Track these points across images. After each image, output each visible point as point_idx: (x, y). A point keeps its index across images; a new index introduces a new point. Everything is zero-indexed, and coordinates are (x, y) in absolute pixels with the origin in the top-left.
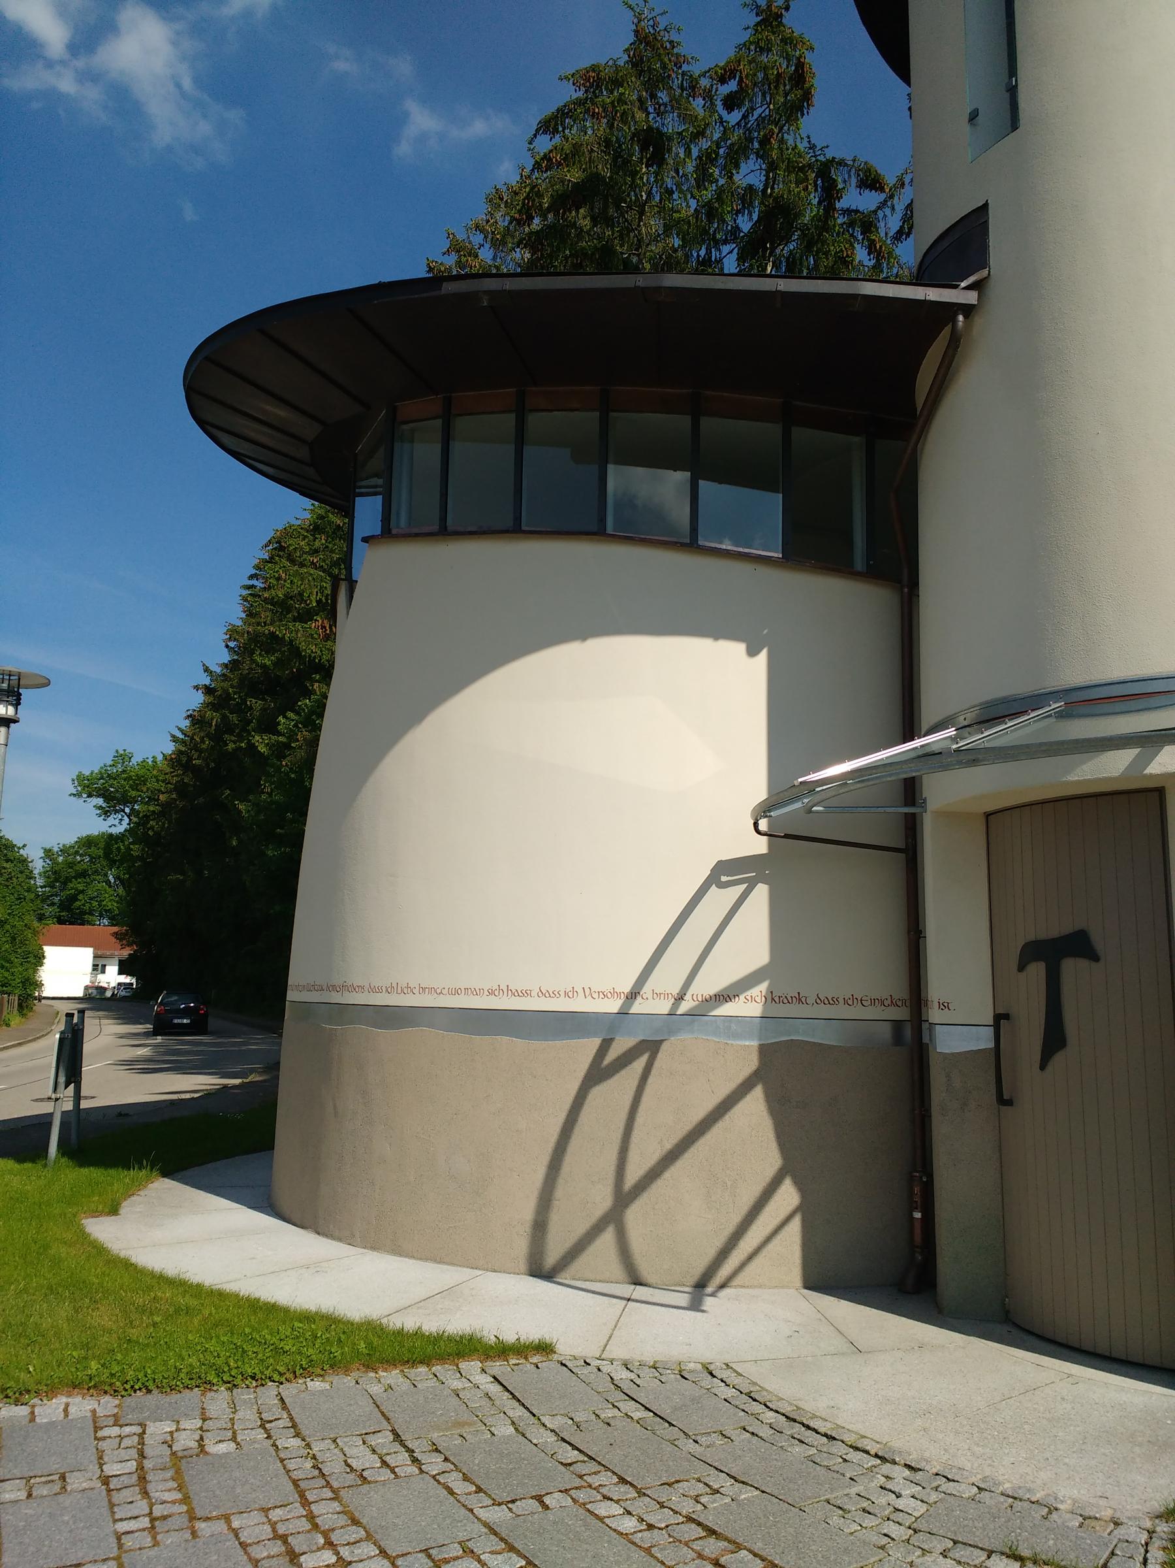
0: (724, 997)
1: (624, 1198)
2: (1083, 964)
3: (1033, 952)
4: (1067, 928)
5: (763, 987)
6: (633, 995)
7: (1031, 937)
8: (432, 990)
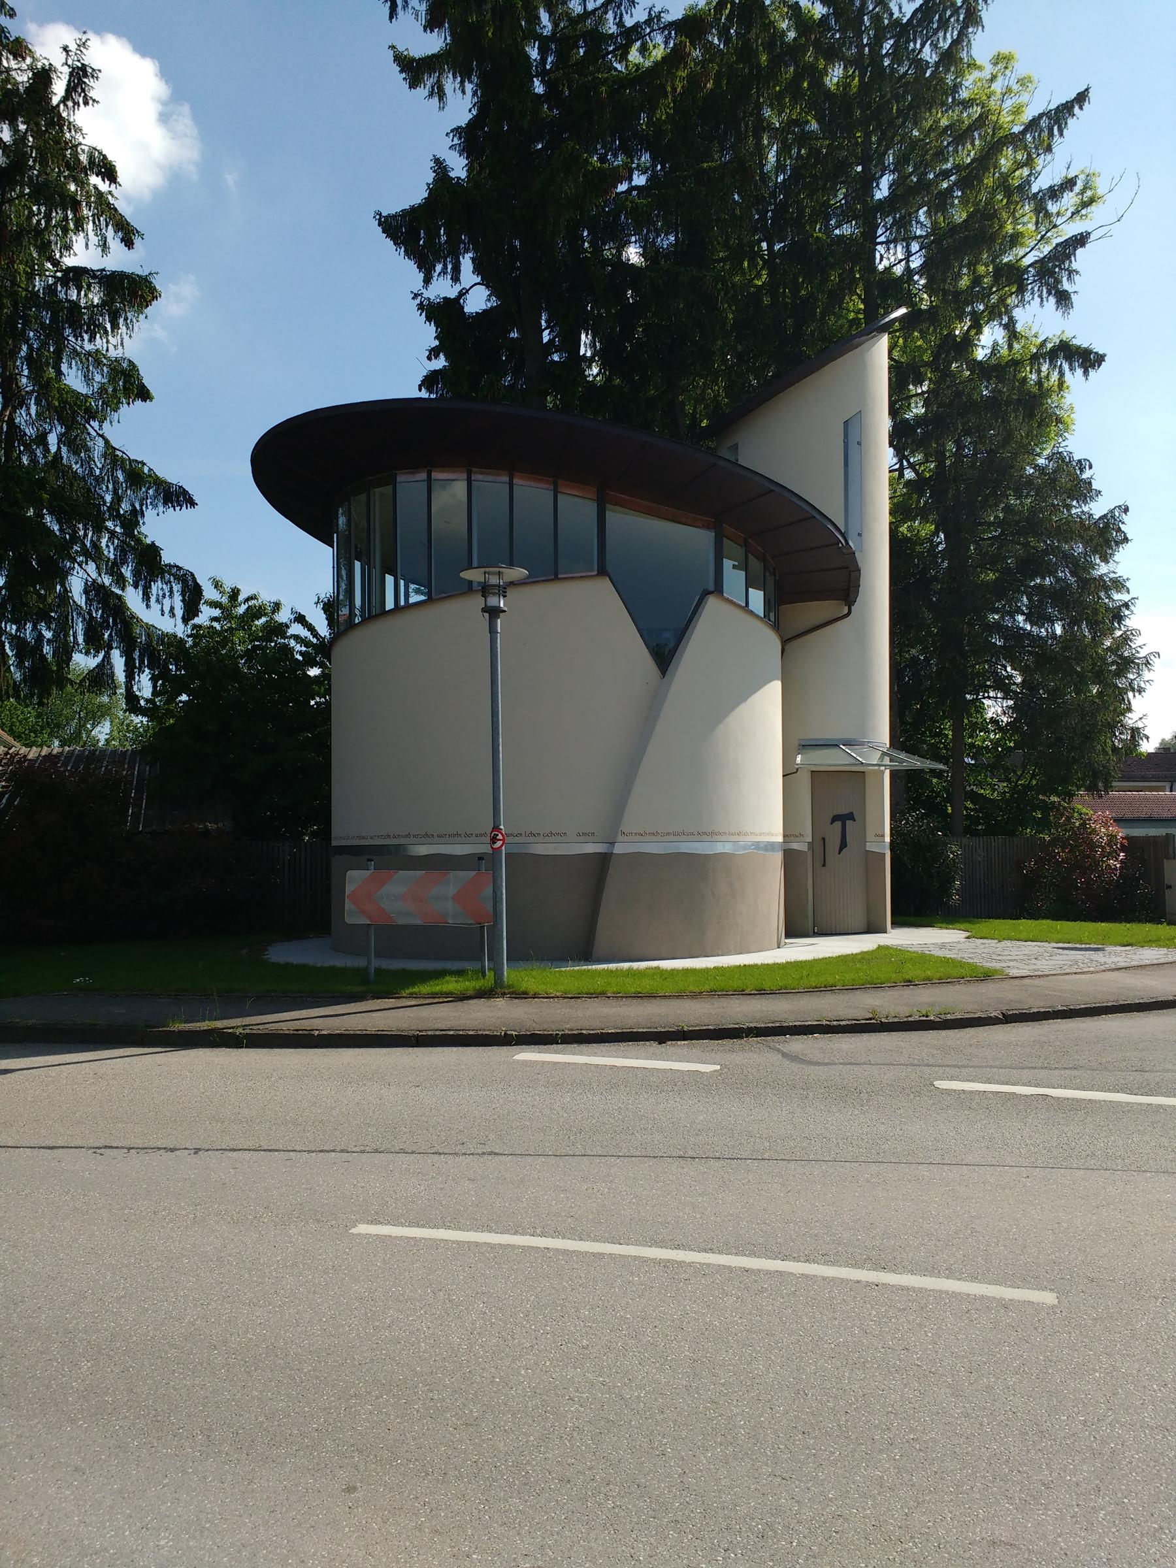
2: (851, 822)
3: (835, 819)
4: (847, 812)
7: (836, 813)
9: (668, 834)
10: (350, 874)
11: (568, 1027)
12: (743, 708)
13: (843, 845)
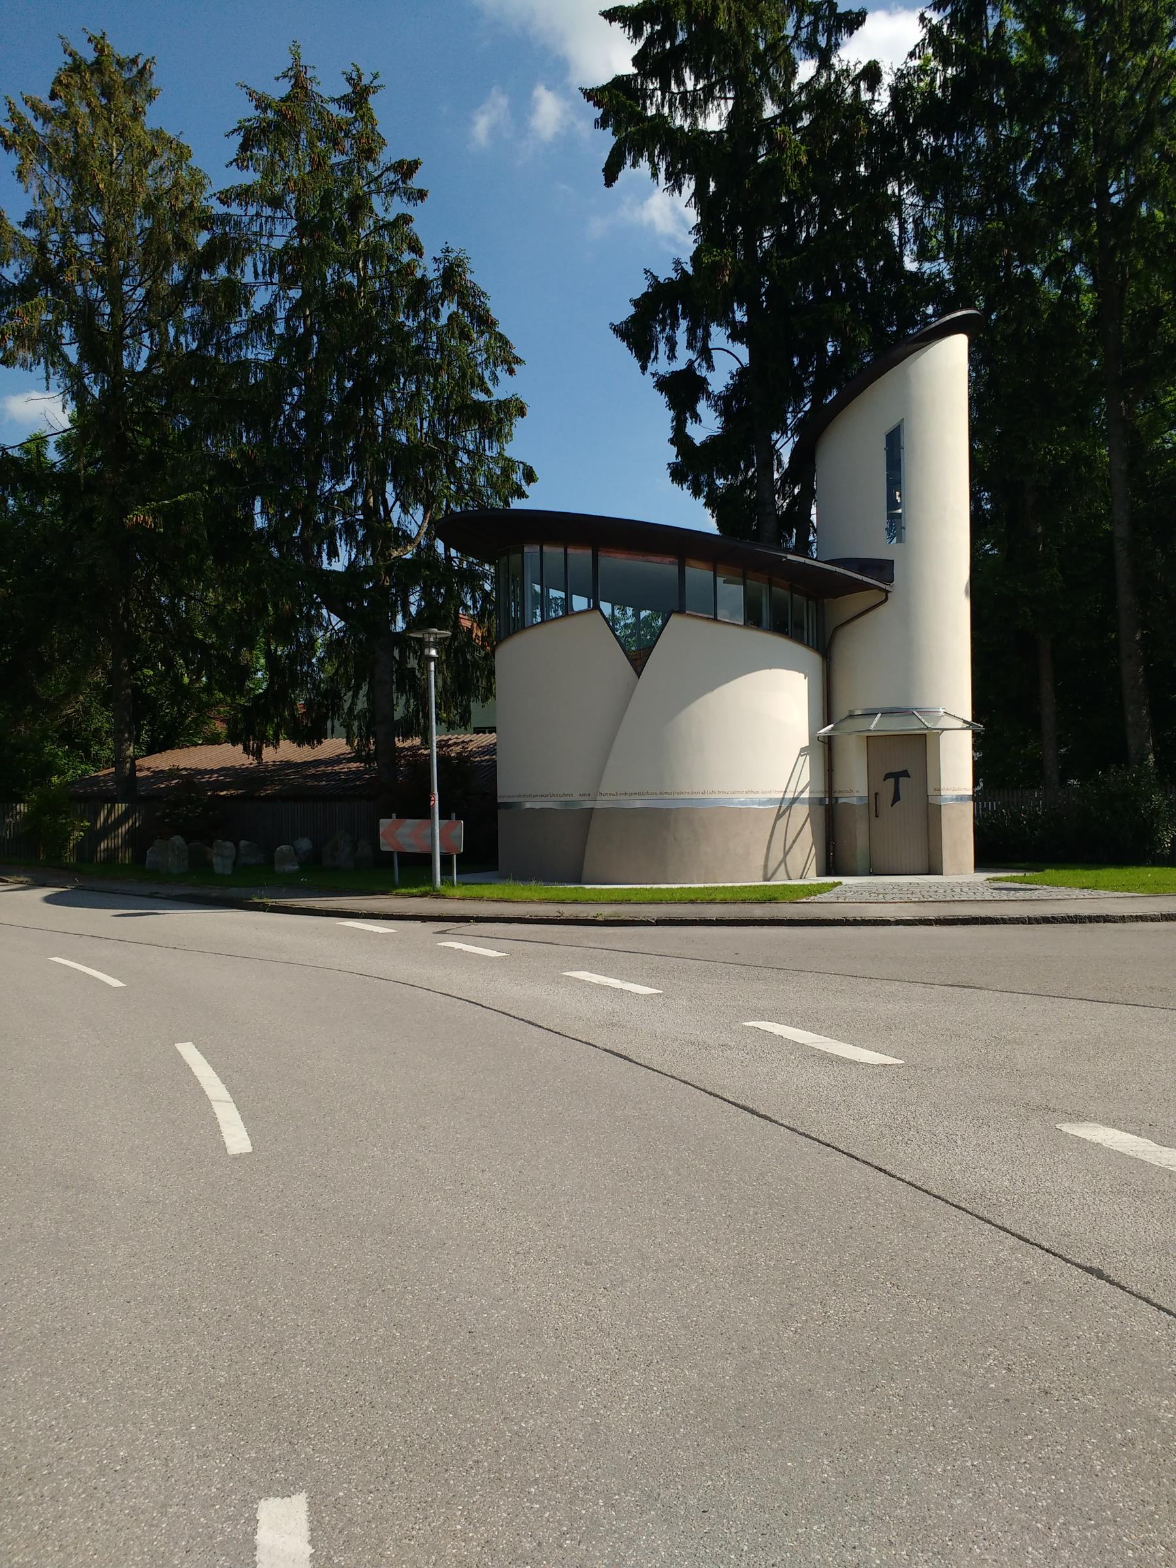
0: (802, 792)
1: (786, 854)
3: (887, 776)
5: (808, 789)
6: (785, 792)
8: (723, 792)
9: (634, 794)
10: (382, 821)
11: (389, 911)
12: (711, 698)
13: (896, 798)
